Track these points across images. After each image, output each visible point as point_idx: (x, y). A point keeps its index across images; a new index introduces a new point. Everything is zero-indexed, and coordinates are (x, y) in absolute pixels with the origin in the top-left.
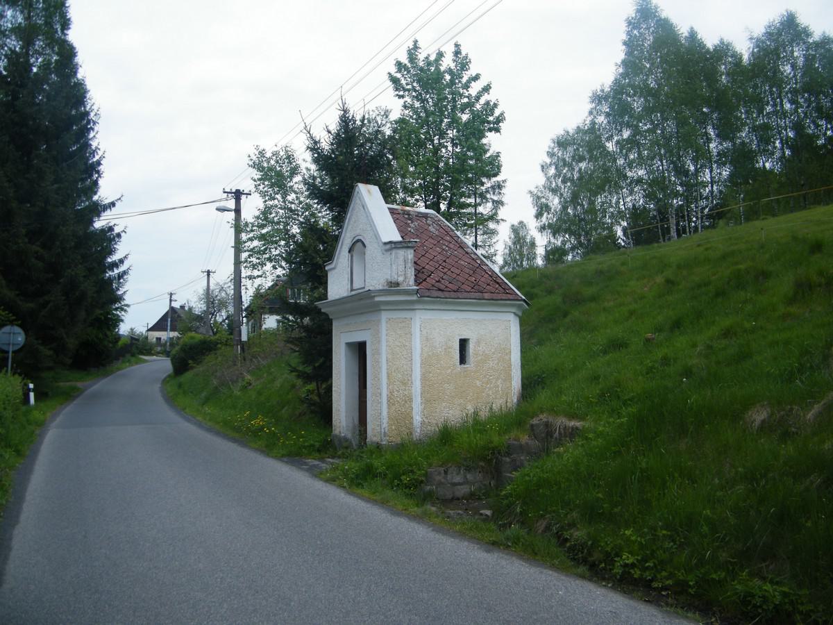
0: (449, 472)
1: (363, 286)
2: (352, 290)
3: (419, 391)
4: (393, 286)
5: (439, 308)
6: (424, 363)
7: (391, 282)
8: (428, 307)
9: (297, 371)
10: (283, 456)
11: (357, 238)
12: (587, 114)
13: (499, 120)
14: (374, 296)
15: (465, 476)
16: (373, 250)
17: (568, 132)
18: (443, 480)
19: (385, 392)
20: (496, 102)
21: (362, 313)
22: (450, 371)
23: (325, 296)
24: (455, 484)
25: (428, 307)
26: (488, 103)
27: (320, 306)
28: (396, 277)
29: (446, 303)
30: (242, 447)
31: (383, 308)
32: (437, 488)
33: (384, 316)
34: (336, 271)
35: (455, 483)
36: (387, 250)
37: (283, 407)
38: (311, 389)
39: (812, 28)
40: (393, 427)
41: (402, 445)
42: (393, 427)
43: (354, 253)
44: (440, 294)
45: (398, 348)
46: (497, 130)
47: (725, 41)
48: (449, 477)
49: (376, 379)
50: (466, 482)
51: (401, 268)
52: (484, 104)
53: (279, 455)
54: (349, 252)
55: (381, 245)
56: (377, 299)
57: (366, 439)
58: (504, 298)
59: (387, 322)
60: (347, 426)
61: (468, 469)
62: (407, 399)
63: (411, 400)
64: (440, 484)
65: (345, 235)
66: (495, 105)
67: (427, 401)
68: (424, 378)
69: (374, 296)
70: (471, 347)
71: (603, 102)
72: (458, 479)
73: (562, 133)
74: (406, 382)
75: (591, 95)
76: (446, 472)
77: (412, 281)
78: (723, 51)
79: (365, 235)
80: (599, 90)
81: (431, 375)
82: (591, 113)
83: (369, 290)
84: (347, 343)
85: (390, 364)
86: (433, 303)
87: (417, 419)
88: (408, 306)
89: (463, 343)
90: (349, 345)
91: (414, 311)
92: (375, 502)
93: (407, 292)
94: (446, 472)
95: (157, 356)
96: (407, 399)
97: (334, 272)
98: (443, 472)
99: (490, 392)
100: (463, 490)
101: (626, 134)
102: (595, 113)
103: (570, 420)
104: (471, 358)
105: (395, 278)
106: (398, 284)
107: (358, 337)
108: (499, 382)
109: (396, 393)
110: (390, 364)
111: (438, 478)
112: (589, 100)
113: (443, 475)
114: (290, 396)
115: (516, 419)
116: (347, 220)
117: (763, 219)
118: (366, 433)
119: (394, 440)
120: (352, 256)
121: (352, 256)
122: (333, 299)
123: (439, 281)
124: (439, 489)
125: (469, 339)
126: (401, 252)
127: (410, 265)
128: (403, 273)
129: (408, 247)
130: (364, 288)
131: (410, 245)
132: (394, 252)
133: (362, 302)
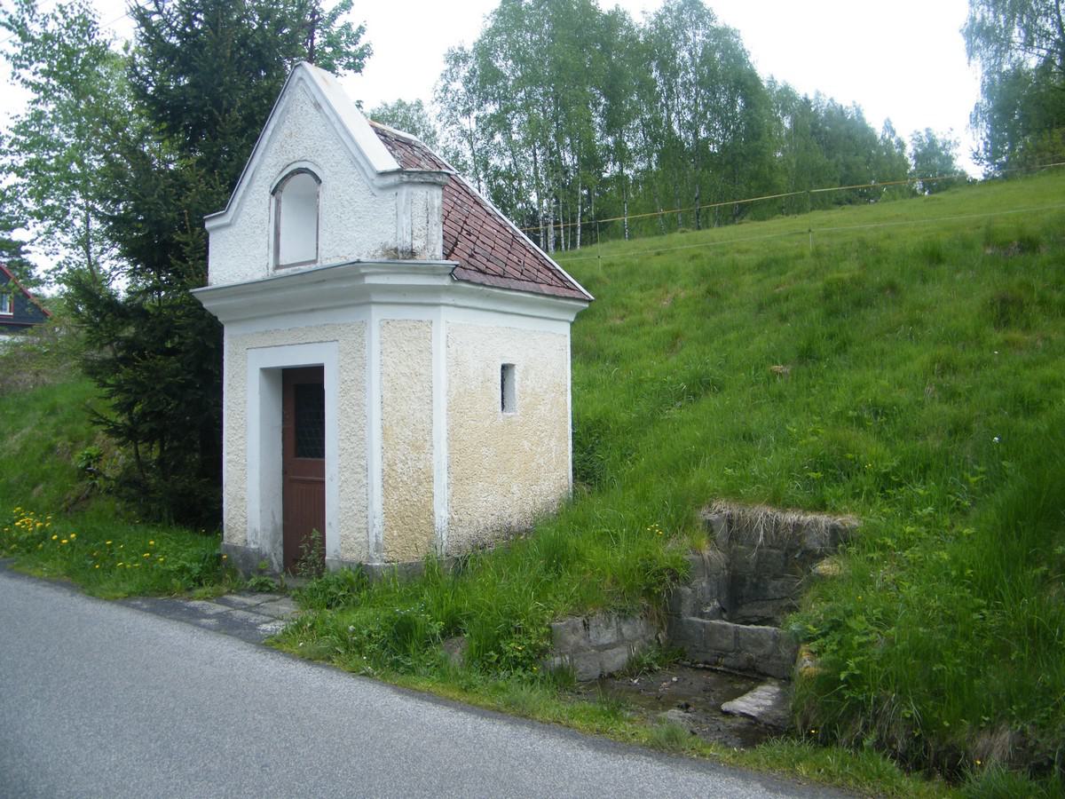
0: (593, 624)
1: (314, 258)
2: (277, 267)
3: (445, 462)
4: (401, 258)
5: (480, 305)
6: (453, 409)
7: (396, 250)
8: (460, 302)
9: (107, 422)
10: (130, 595)
11: (304, 165)
12: (438, 76)
13: (363, 54)
14: (366, 274)
15: (620, 630)
16: (339, 188)
17: (386, 105)
18: (582, 642)
19: (377, 466)
20: (363, 25)
21: (312, 310)
22: (488, 422)
23: (204, 282)
24: (603, 648)
25: (460, 302)
26: (347, 26)
27: (198, 296)
28: (408, 239)
29: (489, 297)
30: (11, 577)
31: (374, 299)
32: (572, 659)
33: (377, 315)
34: (231, 230)
35: (603, 645)
36: (384, 188)
37: (35, 486)
38: (94, 454)
39: (716, 12)
40: (395, 533)
41: (235, 547)
42: (395, 533)
43: (283, 197)
44: (479, 278)
45: (403, 379)
46: (358, 68)
47: (621, 9)
48: (593, 634)
49: (353, 439)
50: (621, 641)
51: (419, 222)
52: (342, 27)
53: (120, 594)
54: (273, 193)
55: (372, 175)
56: (369, 280)
57: (325, 555)
58: (568, 295)
59: (382, 328)
60: (264, 530)
61: (624, 615)
62: (422, 477)
63: (430, 479)
64: (578, 649)
65: (261, 161)
66: (361, 29)
67: (459, 481)
68: (453, 438)
69: (366, 274)
70: (517, 375)
71: (461, 64)
72: (608, 637)
73: (380, 106)
74: (420, 446)
75: (446, 52)
76: (586, 626)
77: (439, 252)
78: (614, 21)
79: (319, 160)
80: (456, 48)
81: (463, 430)
82: (444, 76)
83: (359, 262)
84: (267, 372)
85: (389, 409)
86: (469, 294)
87: (442, 514)
88: (426, 297)
89: (506, 369)
90: (267, 372)
91: (436, 309)
92: (495, 712)
93: (432, 270)
94: (586, 626)
95: (872, 254)
96: (422, 477)
97: (225, 232)
98: (581, 625)
99: (541, 461)
100: (617, 659)
101: (491, 108)
102: (449, 76)
103: (784, 512)
104: (517, 398)
105: (404, 241)
106: (412, 254)
107: (299, 357)
108: (553, 443)
109: (400, 465)
110: (389, 409)
111: (572, 639)
112: (444, 59)
113: (582, 632)
114: (46, 466)
115: (571, 513)
116: (269, 132)
117: (683, 232)
118: (324, 544)
119: (397, 557)
120: (278, 202)
121: (278, 202)
122: (221, 284)
123: (471, 256)
124: (575, 661)
125: (513, 365)
126: (421, 193)
127: (436, 218)
128: (423, 232)
129: (434, 184)
130: (315, 262)
131: (439, 179)
132: (405, 190)
133: (327, 287)
